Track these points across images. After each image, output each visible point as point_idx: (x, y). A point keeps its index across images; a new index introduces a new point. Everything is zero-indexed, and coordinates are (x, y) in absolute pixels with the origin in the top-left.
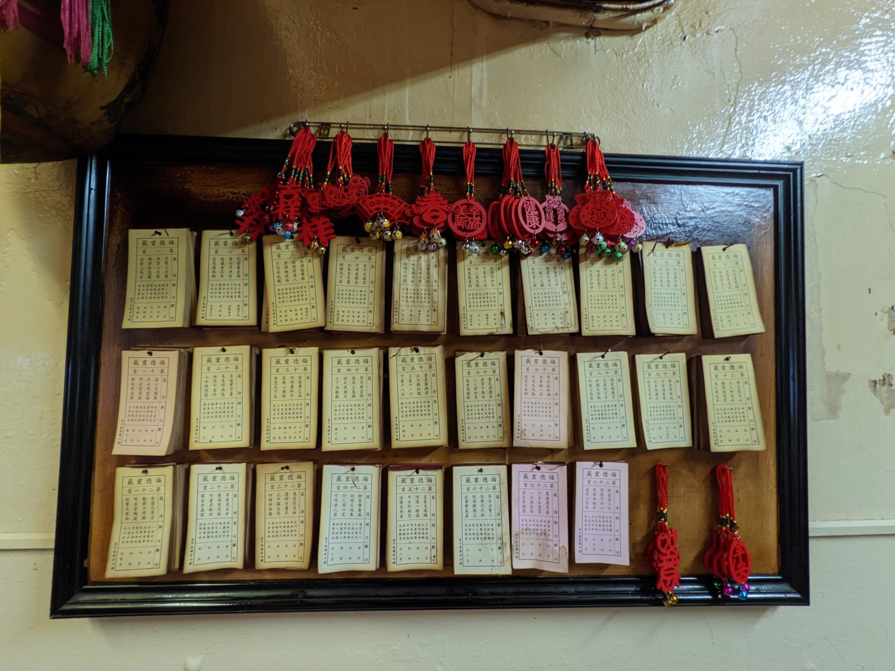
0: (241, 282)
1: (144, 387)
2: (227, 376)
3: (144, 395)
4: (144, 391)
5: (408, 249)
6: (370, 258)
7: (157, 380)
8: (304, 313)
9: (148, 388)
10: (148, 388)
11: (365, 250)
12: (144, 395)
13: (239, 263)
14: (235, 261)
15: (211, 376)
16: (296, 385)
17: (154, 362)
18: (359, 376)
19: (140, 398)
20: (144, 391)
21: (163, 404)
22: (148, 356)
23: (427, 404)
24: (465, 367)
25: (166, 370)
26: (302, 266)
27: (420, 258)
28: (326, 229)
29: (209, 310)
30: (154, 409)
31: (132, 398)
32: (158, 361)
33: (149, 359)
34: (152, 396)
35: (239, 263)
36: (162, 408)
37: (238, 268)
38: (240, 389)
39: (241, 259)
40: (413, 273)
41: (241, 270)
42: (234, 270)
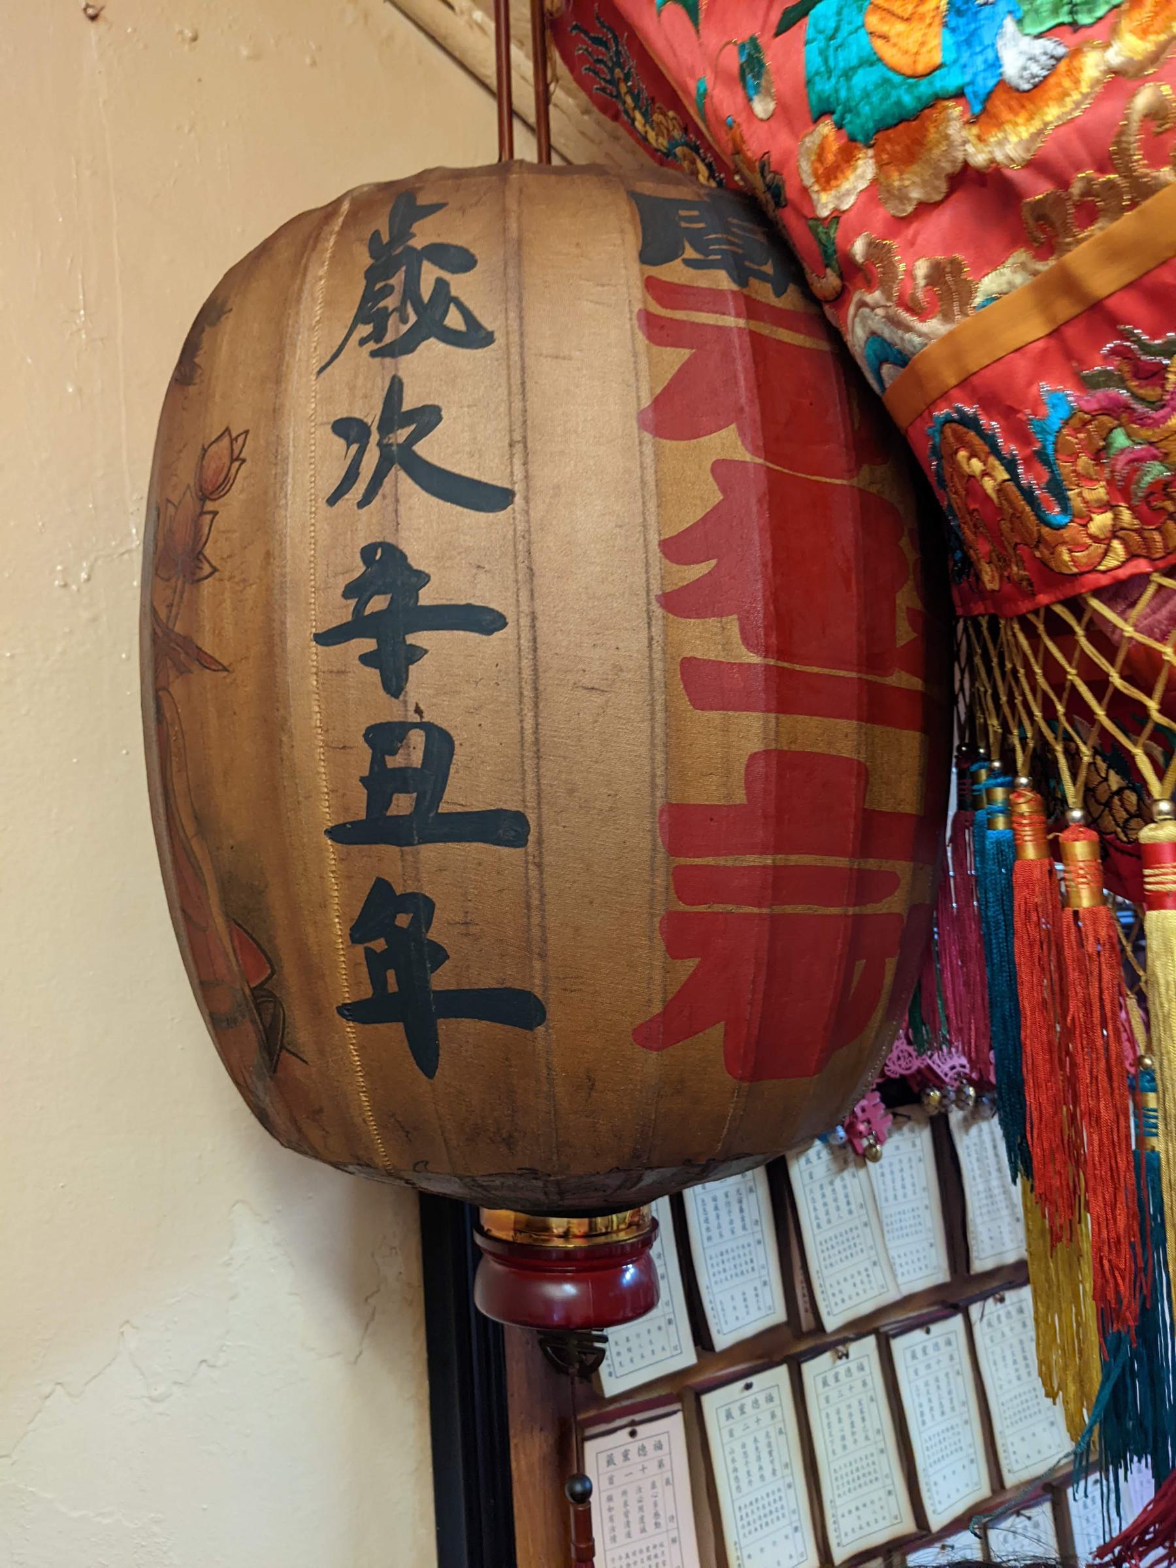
0: (750, 1240)
1: (633, 1507)
2: (761, 1436)
3: (635, 1527)
4: (634, 1516)
5: (965, 1119)
6: (914, 1145)
7: (654, 1486)
8: (865, 1279)
9: (641, 1509)
10: (641, 1509)
11: (905, 1129)
12: (635, 1527)
13: (740, 1201)
14: (733, 1199)
15: (832, 1411)
16: (857, 1418)
17: (642, 1450)
18: (763, 1433)
19: (629, 1535)
20: (634, 1516)
21: (674, 1534)
22: (630, 1439)
23: (1033, 1394)
24: (910, 1362)
25: (666, 1462)
26: (845, 1187)
27: (980, 1130)
28: (1156, 1118)
29: (721, 1313)
30: (659, 1551)
31: (614, 1539)
32: (649, 1445)
33: (633, 1446)
34: (650, 1521)
35: (740, 1201)
36: (674, 1541)
37: (741, 1210)
38: (786, 1459)
39: (743, 1191)
40: (978, 1160)
41: (746, 1214)
42: (736, 1215)
